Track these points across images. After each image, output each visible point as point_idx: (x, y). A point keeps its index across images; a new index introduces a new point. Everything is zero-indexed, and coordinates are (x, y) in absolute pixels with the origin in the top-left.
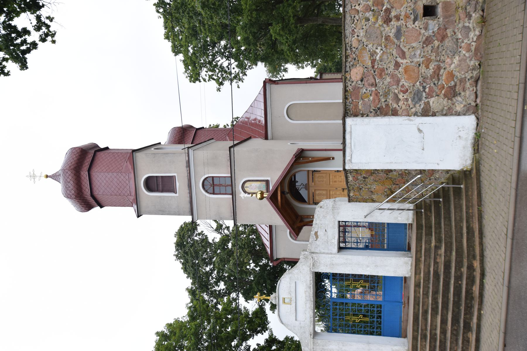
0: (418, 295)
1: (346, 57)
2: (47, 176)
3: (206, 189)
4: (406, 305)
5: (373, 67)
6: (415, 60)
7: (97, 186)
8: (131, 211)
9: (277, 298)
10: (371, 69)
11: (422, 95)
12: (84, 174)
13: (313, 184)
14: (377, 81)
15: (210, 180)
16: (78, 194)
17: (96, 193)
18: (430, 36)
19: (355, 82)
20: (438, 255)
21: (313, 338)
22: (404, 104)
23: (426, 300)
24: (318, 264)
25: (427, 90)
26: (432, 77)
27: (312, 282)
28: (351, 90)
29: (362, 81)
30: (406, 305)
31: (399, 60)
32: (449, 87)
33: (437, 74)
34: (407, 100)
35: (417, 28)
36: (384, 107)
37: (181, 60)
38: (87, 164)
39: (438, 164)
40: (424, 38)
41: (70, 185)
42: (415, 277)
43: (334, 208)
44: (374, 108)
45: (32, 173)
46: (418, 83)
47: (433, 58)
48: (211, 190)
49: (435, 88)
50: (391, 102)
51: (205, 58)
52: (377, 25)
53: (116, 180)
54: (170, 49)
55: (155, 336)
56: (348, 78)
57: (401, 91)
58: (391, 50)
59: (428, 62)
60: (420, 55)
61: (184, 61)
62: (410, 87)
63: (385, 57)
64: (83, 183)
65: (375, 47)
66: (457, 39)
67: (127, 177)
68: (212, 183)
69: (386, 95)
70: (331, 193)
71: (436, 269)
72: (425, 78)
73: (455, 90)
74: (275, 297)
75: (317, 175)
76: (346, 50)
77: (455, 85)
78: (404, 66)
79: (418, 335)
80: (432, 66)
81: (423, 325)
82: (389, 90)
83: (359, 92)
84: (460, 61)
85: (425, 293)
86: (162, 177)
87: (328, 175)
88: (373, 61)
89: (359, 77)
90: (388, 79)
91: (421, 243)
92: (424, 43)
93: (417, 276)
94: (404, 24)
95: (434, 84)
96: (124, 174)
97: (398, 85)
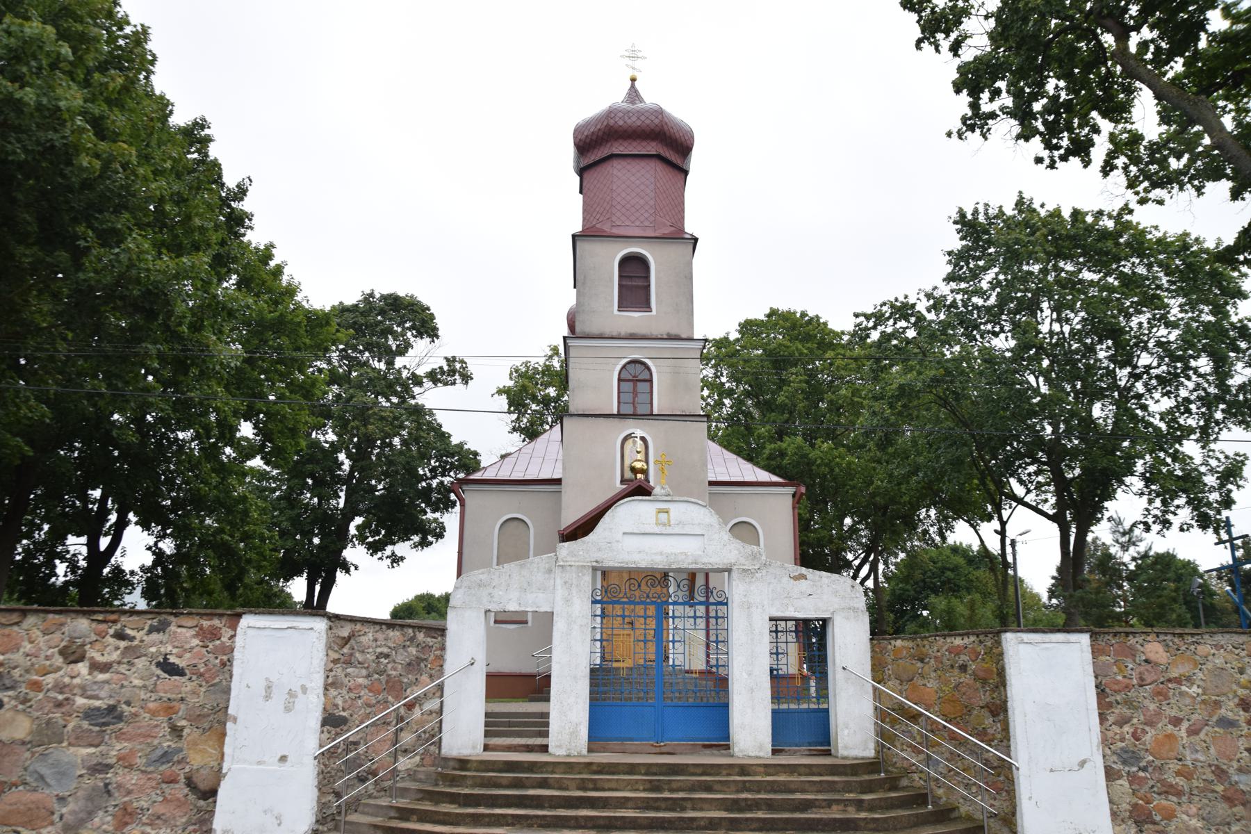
0: (724, 772)
1: (1181, 635)
2: (633, 80)
3: (628, 367)
4: (658, 750)
5: (1170, 680)
6: (1187, 752)
7: (629, 167)
9: (669, 498)
10: (1167, 678)
11: (1133, 765)
12: (652, 148)
14: (1147, 687)
15: (645, 376)
16: (616, 131)
17: (616, 165)
18: (1229, 777)
19: (1142, 649)
20: (845, 806)
22: (1116, 734)
23: (733, 788)
24: (747, 580)
25: (1141, 774)
26: (1163, 782)
27: (633, 566)
28: (1129, 643)
29: (1146, 661)
30: (655, 750)
31: (1185, 725)
32: (1151, 812)
33: (1169, 790)
34: (1123, 739)
35: (1239, 756)
36: (1107, 700)
37: (727, 334)
38: (668, 155)
39: (1030, 798)
40: (1225, 767)
41: (634, 119)
43: (855, 610)
44: (1103, 682)
45: (640, 55)
46: (1151, 758)
47: (1195, 784)
48: (625, 375)
49: (1146, 788)
50: (1116, 711)
51: (337, 349)
52: (1235, 687)
53: (642, 202)
54: (751, 317)
56: (1149, 638)
57: (1136, 729)
58: (1199, 711)
59: (1185, 774)
60: (1195, 760)
61: (726, 339)
62: (1145, 745)
63: (1188, 701)
64: (635, 144)
65: (1200, 683)
66: (1229, 824)
67: (647, 223)
68: (639, 378)
69: (1128, 703)
71: (817, 803)
72: (1160, 769)
73: (1147, 823)
74: (669, 495)
76: (1193, 635)
77: (1154, 823)
78: (1176, 733)
80: (1180, 782)
81: (679, 784)
82: (1136, 708)
83: (1126, 657)
84: (1195, 829)
85: (747, 784)
86: (649, 286)
88: (1178, 681)
89: (1152, 657)
90: (1152, 707)
92: (1217, 767)
93: (762, 769)
94: (1243, 733)
95: (1153, 787)
96: (652, 219)
97: (1145, 724)
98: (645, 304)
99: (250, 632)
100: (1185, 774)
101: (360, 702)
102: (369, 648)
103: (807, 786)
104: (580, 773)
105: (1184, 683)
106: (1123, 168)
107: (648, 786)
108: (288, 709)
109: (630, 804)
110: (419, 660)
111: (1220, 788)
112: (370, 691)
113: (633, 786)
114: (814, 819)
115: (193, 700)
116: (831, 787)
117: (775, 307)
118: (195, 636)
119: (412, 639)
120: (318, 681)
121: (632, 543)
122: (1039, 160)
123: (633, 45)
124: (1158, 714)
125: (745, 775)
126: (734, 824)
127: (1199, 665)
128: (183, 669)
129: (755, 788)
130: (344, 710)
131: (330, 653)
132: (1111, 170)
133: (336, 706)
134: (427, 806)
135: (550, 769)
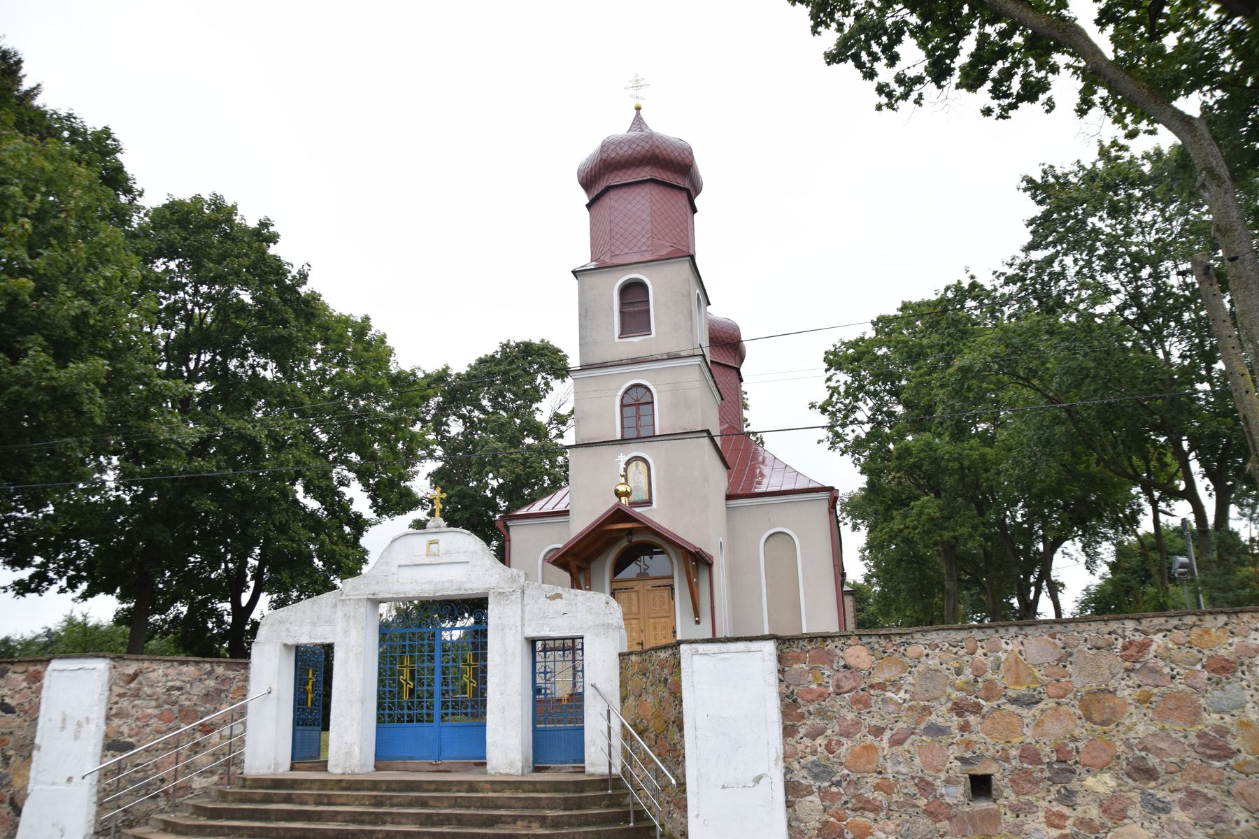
0: (454, 789)
1: (887, 636)
2: (638, 109)
4: (435, 768)
5: (872, 687)
6: (889, 764)
8: (584, 258)
9: (437, 530)
12: (646, 173)
13: (649, 588)
14: (845, 695)
16: (610, 164)
17: (613, 195)
19: (841, 654)
20: (529, 822)
21: (368, 599)
22: (807, 747)
24: (502, 603)
25: (834, 789)
26: (858, 797)
27: (470, 592)
28: (827, 648)
29: (845, 667)
33: (865, 806)
34: (814, 752)
35: (948, 765)
36: (799, 711)
39: (697, 816)
40: (930, 779)
41: (625, 148)
42: (486, 782)
43: (607, 626)
44: (795, 691)
46: (846, 772)
47: (895, 797)
48: (628, 401)
49: (839, 804)
50: (808, 723)
52: (949, 690)
53: (639, 228)
55: (363, 315)
56: (849, 642)
58: (904, 719)
59: (886, 787)
60: (898, 773)
62: (839, 758)
63: (891, 708)
64: (629, 172)
65: (908, 688)
69: (822, 713)
70: (634, 622)
71: (503, 819)
72: (856, 783)
75: (666, 593)
76: (901, 635)
78: (876, 744)
79: (381, 790)
80: (880, 796)
81: (400, 799)
82: (830, 718)
85: (459, 800)
86: (648, 311)
87: (637, 616)
88: (882, 686)
89: (852, 661)
90: (850, 716)
91: (549, 792)
92: (921, 779)
93: (488, 786)
94: (954, 741)
95: (846, 802)
98: (645, 328)
99: (55, 674)
100: (886, 787)
101: (148, 730)
102: (158, 682)
103: (513, 802)
104: (332, 789)
105: (888, 688)
106: (1101, 103)
107: (373, 801)
108: (76, 738)
109: (340, 818)
110: (219, 692)
111: (922, 802)
112: (160, 719)
113: (359, 801)
114: (479, 834)
115: (18, 733)
116: (536, 804)
117: (906, 300)
118: (24, 680)
119: (210, 673)
120: (99, 713)
121: (406, 574)
122: (987, 112)
123: (637, 75)
124: (857, 724)
125: (473, 791)
126: (200, 830)
127: (908, 669)
128: (14, 708)
129: (466, 804)
130: (130, 736)
131: (114, 688)
132: (1090, 108)
133: (122, 733)
134: (203, 821)
135: (308, 786)
